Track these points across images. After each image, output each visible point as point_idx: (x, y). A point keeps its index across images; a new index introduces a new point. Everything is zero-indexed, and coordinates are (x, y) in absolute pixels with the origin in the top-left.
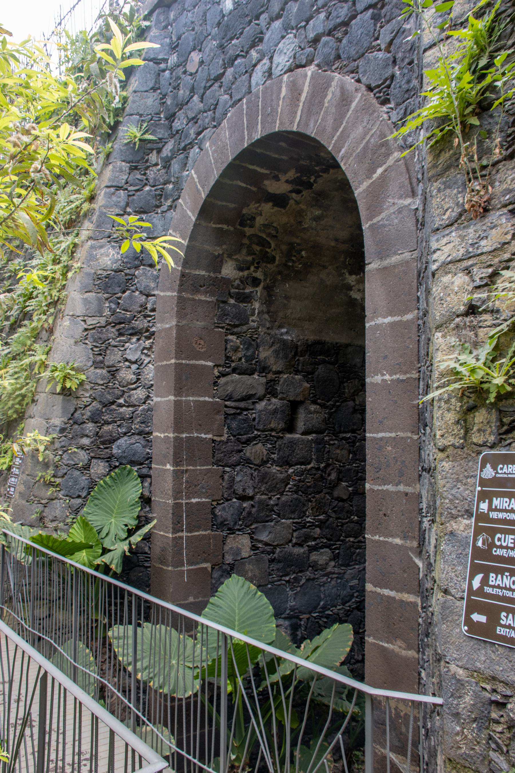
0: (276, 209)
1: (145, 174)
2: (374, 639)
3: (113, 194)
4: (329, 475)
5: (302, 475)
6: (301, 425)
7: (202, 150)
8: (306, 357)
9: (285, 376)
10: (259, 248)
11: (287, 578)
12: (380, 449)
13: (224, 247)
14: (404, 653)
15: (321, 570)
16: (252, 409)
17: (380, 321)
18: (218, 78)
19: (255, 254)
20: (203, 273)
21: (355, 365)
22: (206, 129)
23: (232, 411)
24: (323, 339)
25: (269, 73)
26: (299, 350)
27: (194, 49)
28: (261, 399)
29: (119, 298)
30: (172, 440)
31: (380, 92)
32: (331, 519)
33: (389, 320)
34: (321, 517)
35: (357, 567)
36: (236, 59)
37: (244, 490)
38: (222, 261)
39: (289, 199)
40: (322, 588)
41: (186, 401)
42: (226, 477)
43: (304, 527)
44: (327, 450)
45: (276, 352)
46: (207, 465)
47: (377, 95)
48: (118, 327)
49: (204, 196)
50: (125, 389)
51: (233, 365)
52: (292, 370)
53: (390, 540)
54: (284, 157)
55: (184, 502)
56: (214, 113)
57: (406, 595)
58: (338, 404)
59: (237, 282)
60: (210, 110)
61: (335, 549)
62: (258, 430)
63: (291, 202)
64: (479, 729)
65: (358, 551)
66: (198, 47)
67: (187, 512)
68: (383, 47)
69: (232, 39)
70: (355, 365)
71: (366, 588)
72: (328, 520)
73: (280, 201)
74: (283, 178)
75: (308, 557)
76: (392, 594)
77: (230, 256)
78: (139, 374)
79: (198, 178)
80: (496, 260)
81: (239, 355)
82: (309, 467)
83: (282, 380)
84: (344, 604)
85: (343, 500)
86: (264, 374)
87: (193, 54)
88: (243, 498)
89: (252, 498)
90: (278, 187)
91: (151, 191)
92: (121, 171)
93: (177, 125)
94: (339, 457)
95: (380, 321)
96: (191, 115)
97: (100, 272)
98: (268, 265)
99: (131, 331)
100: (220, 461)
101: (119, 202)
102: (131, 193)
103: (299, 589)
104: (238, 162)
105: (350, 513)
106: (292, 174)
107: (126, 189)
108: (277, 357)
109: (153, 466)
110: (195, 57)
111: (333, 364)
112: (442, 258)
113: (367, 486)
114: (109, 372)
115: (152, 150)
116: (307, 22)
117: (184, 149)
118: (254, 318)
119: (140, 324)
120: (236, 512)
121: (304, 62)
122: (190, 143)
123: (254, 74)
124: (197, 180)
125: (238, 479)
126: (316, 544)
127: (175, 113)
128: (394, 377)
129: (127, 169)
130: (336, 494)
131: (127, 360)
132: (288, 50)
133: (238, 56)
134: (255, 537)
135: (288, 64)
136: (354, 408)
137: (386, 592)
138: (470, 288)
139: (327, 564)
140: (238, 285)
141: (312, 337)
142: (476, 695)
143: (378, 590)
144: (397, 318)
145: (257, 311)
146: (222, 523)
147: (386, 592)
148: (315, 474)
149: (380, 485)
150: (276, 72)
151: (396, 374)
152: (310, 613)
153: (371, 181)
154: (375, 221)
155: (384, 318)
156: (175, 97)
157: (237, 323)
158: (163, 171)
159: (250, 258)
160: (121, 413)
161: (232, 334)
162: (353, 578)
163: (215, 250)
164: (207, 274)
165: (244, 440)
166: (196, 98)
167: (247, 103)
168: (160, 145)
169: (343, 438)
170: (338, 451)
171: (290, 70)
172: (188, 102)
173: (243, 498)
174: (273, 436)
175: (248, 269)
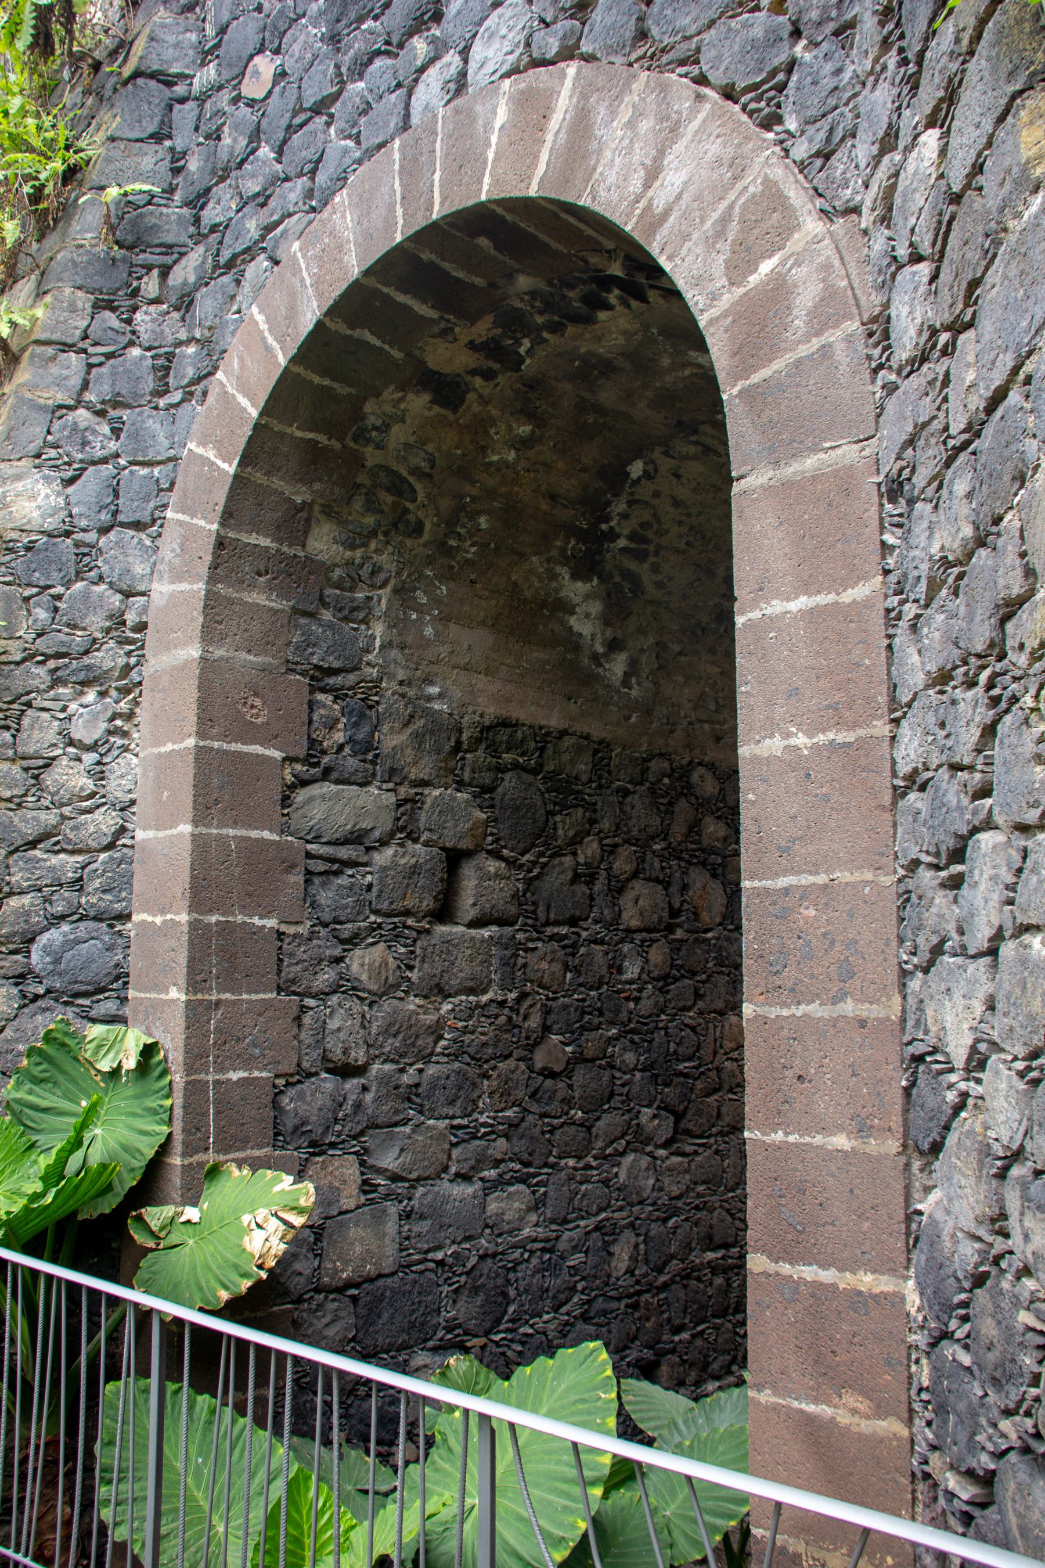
0: (436, 409)
1: (129, 322)
2: (775, 1394)
3: (53, 359)
4: (526, 1017)
5: (470, 1017)
6: (467, 905)
7: (277, 263)
8: (480, 752)
9: (437, 792)
10: (389, 499)
11: (439, 1255)
12: (785, 915)
13: (317, 486)
14: (865, 1426)
15: (510, 1232)
16: (365, 865)
17: (776, 607)
18: (320, 107)
19: (382, 512)
20: (265, 542)
21: (577, 778)
22: (290, 215)
23: (320, 866)
24: (515, 715)
25: (460, 84)
26: (465, 737)
27: (260, 51)
28: (384, 843)
29: (58, 597)
30: (186, 929)
31: (758, 99)
32: (530, 1118)
33: (803, 602)
34: (508, 1113)
35: (582, 1223)
36: (370, 61)
37: (346, 1051)
38: (308, 520)
39: (467, 391)
40: (511, 1275)
41: (219, 838)
42: (307, 1020)
44: (520, 961)
45: (418, 737)
46: (264, 991)
47: (753, 106)
48: (52, 664)
49: (282, 361)
50: (67, 810)
51: (326, 760)
52: (450, 780)
53: (818, 1139)
54: (479, 281)
55: (210, 1078)
56: (313, 179)
57: (869, 1278)
58: (543, 860)
59: (338, 572)
60: (301, 175)
61: (537, 1185)
62: (376, 912)
63: (471, 396)
65: (584, 1187)
66: (273, 41)
67: (217, 1102)
69: (361, 20)
70: (577, 778)
71: (749, 1265)
72: (523, 1119)
73: (447, 391)
74: (464, 333)
75: (483, 1206)
76: (828, 1276)
77: (328, 511)
78: (101, 776)
79: (268, 320)
81: (339, 737)
82: (484, 998)
83: (429, 801)
84: (556, 1309)
85: (552, 1075)
86: (391, 785)
87: (257, 60)
88: (345, 1071)
89: (360, 1071)
90: (447, 356)
91: (142, 358)
92: (73, 309)
93: (212, 214)
94: (546, 979)
95: (776, 607)
96: (252, 187)
97: (14, 535)
98: (409, 542)
99: (82, 676)
100: (293, 981)
101: (66, 378)
102: (94, 360)
103: (463, 1279)
104: (373, 282)
105: (568, 1102)
106: (483, 329)
107: (85, 351)
108: (419, 748)
109: (131, 993)
110: (265, 66)
111: (535, 772)
113: (748, 1009)
114: (26, 770)
115: (149, 268)
117: (230, 265)
118: (370, 657)
119: (109, 657)
120: (329, 1103)
123: (421, 87)
124: (264, 326)
125: (333, 1024)
126: (500, 1175)
127: (208, 190)
129: (88, 306)
130: (540, 1059)
131: (71, 743)
132: (510, 29)
133: (378, 53)
134: (371, 1161)
135: (512, 58)
136: (575, 870)
137: (809, 1272)
139: (521, 1219)
140: (341, 578)
141: (491, 710)
144: (823, 599)
145: (378, 643)
146: (296, 1129)
147: (809, 1272)
148: (497, 1016)
149: (785, 1005)
150: (478, 77)
151: (824, 731)
152: (487, 1333)
153: (742, 290)
154: (756, 378)
155: (788, 600)
157: (336, 664)
158: (176, 315)
159: (370, 520)
160: (52, 869)
161: (323, 690)
162: (575, 1249)
163: (297, 493)
164: (274, 545)
165: (346, 935)
166: (265, 152)
167: (402, 148)
168: (168, 260)
169: (552, 938)
170: (544, 965)
171: (515, 71)
172: (243, 161)
173: (345, 1071)
174: (409, 927)
175: (365, 545)
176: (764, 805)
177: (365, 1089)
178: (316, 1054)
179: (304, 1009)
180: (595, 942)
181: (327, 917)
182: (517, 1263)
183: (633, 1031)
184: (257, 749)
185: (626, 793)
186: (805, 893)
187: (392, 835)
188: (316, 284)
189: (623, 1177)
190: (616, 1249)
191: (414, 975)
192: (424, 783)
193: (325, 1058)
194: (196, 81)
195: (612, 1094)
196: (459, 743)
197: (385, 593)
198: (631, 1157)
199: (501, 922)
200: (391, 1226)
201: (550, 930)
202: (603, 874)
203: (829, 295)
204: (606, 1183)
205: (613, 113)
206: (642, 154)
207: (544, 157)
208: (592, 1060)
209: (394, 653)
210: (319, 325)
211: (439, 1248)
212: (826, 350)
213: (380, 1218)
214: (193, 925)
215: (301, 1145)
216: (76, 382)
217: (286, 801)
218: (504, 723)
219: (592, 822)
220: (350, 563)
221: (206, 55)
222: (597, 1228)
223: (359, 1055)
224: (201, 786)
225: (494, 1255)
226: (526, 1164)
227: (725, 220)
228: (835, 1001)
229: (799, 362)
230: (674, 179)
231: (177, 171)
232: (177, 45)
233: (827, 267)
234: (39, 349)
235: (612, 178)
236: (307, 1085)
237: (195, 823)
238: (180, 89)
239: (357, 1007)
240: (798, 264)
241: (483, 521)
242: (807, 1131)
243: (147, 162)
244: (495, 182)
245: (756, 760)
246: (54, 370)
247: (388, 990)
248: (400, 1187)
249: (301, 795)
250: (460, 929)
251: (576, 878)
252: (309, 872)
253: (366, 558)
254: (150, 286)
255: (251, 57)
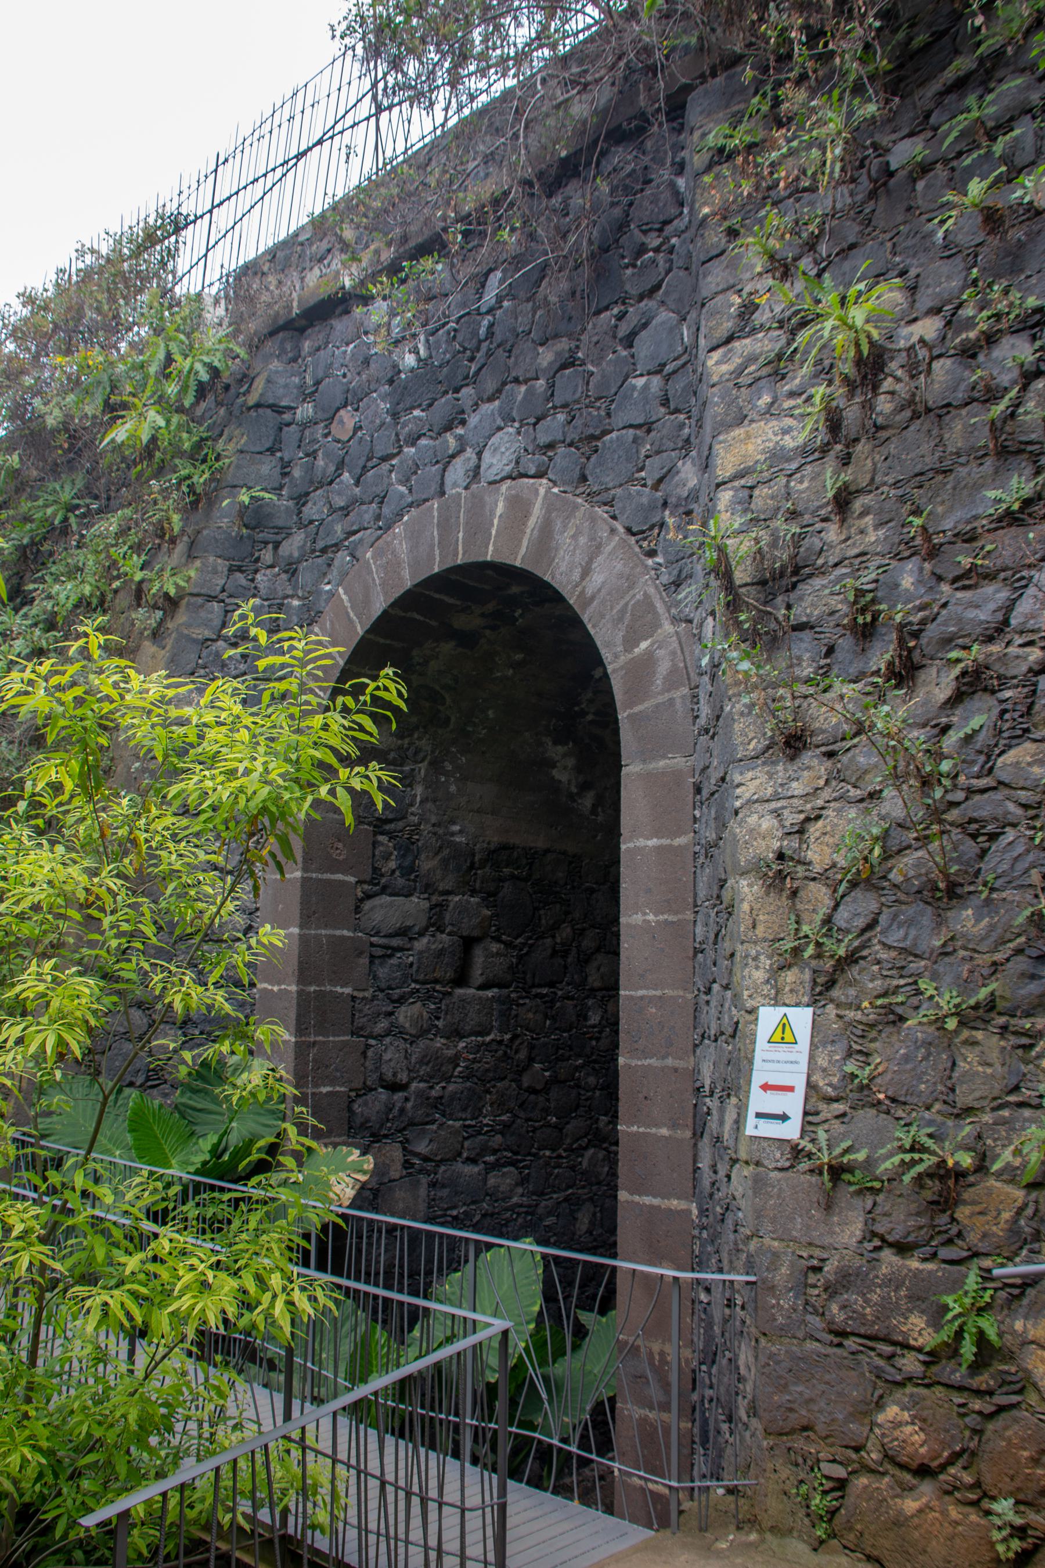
1: (253, 580)
6: (477, 975)
11: (455, 1213)
15: (503, 1200)
17: (641, 842)
23: (379, 952)
28: (421, 934)
33: (653, 842)
37: (395, 1074)
41: (316, 936)
42: (370, 1053)
43: (479, 1133)
45: (445, 862)
49: (360, 631)
51: (383, 880)
53: (654, 1130)
59: (392, 755)
62: (416, 981)
64: (796, 1297)
68: (649, 483)
69: (413, 408)
73: (466, 639)
76: (656, 1201)
80: (809, 806)
81: (392, 865)
82: (488, 1039)
87: (342, 412)
88: (394, 1087)
89: (404, 1087)
92: (215, 572)
93: (310, 511)
95: (641, 842)
96: (340, 502)
100: (362, 1028)
105: (546, 1111)
112: (747, 795)
113: (621, 1060)
115: (266, 543)
116: (538, 420)
117: (324, 551)
121: (532, 472)
122: (336, 545)
124: (347, 604)
125: (387, 1057)
127: (307, 494)
128: (661, 918)
130: (526, 1081)
137: (647, 1200)
138: (779, 834)
142: (792, 1265)
143: (636, 1198)
147: (647, 1200)
154: (637, 709)
156: (310, 468)
158: (284, 576)
162: (550, 1214)
168: (279, 538)
169: (536, 996)
170: (530, 1015)
173: (394, 1087)
176: (633, 951)
177: (407, 1099)
178: (375, 1076)
179: (368, 1046)
180: (568, 998)
181: (383, 985)
182: (508, 1221)
183: (595, 1061)
184: (339, 877)
185: (592, 891)
186: (651, 999)
187: (426, 929)
188: (383, 584)
189: (585, 1164)
190: (579, 1215)
191: (440, 1024)
192: (448, 893)
193: (381, 1079)
194: (299, 411)
195: (578, 1106)
196: (473, 863)
197: (424, 766)
198: (591, 1151)
199: (500, 986)
200: (423, 1191)
201: (534, 991)
202: (574, 951)
203: (674, 670)
204: (572, 1168)
205: (565, 527)
206: (580, 558)
207: (525, 543)
208: (564, 1082)
209: (429, 805)
210: (385, 612)
211: (455, 1207)
212: (671, 701)
213: (416, 1184)
214: (300, 993)
215: (366, 1134)
216: (217, 623)
217: (357, 910)
218: (504, 847)
219: (567, 913)
220: (400, 748)
221: (306, 395)
222: (566, 1199)
223: (403, 1077)
224: (305, 901)
225: (492, 1215)
226: (516, 1153)
227: (623, 611)
228: (663, 1058)
229: (657, 706)
230: (597, 579)
231: (285, 475)
232: (286, 386)
233: (673, 653)
234: (193, 600)
235: (563, 568)
236: (369, 1097)
237: (301, 927)
238: (287, 417)
239: (402, 1045)
240: (659, 648)
241: (491, 713)
242: (648, 1126)
243: (265, 469)
244: (495, 550)
245: (629, 925)
246: (203, 614)
247: (423, 1033)
248: (429, 1166)
249: (367, 905)
250: (472, 991)
251: (554, 953)
252: (372, 956)
253: (410, 744)
254: (267, 556)
255: (338, 410)
